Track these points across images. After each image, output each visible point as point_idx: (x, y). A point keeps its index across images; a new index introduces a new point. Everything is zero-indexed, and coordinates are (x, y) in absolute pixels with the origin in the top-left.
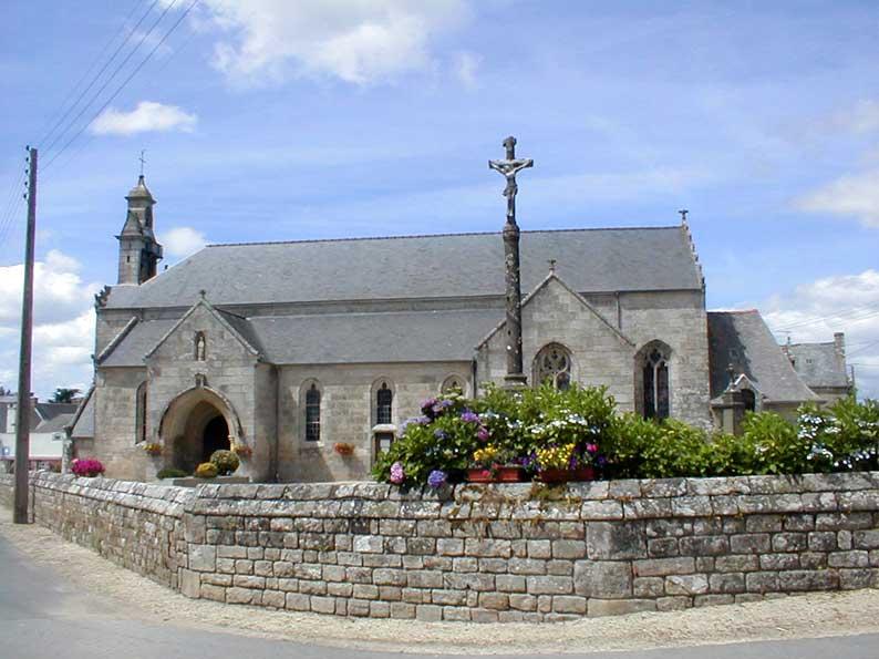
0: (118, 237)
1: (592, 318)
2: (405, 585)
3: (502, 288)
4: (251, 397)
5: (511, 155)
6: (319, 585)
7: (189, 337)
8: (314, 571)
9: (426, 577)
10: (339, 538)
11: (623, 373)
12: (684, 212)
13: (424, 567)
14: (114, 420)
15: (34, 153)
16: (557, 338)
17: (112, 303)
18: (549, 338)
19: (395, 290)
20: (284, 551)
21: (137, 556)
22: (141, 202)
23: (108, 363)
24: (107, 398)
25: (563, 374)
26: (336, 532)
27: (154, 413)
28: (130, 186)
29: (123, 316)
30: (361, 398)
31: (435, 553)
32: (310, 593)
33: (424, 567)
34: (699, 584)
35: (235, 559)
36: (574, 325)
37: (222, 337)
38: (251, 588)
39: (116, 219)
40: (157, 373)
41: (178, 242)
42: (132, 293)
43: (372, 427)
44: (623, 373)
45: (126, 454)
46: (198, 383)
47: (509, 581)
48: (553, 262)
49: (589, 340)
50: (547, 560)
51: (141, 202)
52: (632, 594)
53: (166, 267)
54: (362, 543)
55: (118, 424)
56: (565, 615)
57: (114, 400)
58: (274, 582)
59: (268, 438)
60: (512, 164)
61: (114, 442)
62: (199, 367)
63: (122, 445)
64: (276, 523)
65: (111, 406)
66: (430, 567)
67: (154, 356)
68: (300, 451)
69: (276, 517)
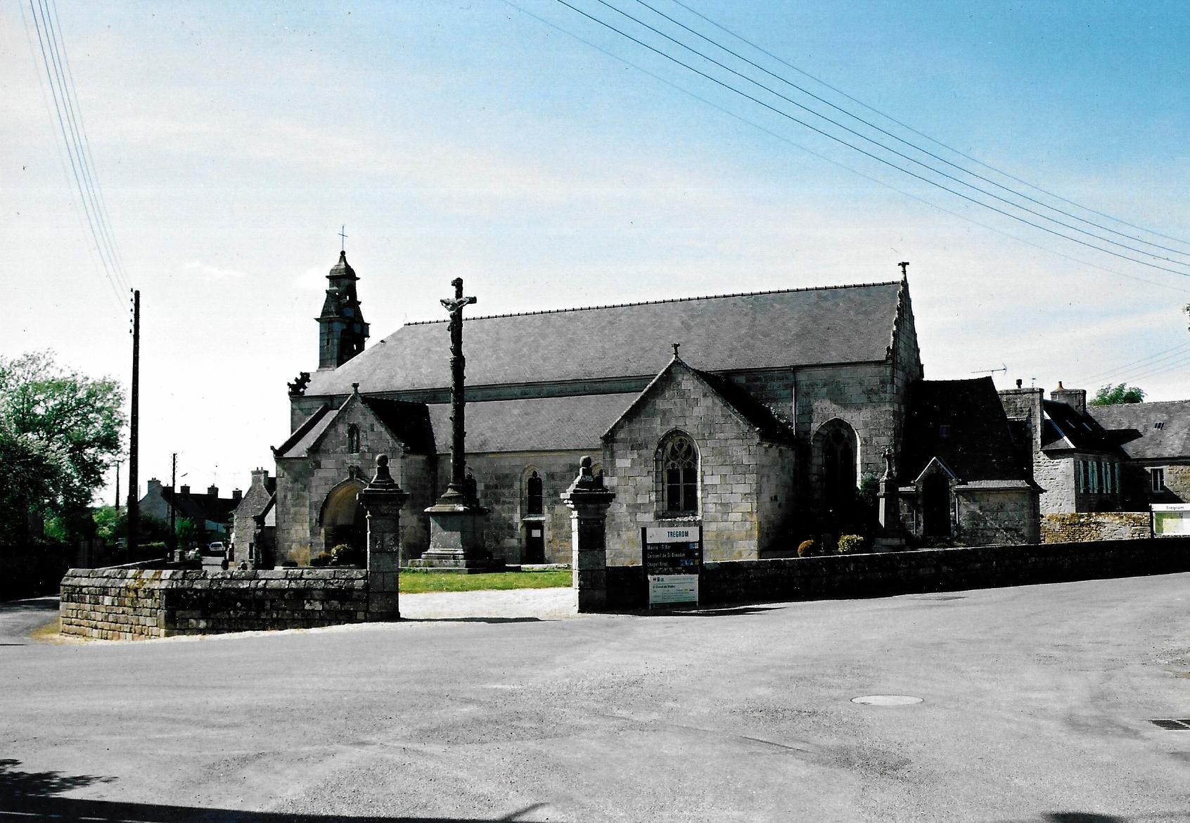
3: (469, 408)
7: (343, 429)
11: (745, 462)
12: (904, 265)
15: (137, 294)
17: (311, 389)
18: (672, 426)
19: (571, 369)
21: (99, 616)
22: (343, 282)
23: (291, 453)
25: (689, 464)
28: (333, 262)
30: (511, 486)
34: (203, 624)
36: (698, 411)
41: (381, 314)
42: (338, 380)
44: (745, 462)
46: (352, 474)
49: (710, 426)
51: (343, 282)
52: (175, 625)
54: (107, 600)
55: (295, 514)
57: (292, 490)
61: (293, 531)
62: (354, 460)
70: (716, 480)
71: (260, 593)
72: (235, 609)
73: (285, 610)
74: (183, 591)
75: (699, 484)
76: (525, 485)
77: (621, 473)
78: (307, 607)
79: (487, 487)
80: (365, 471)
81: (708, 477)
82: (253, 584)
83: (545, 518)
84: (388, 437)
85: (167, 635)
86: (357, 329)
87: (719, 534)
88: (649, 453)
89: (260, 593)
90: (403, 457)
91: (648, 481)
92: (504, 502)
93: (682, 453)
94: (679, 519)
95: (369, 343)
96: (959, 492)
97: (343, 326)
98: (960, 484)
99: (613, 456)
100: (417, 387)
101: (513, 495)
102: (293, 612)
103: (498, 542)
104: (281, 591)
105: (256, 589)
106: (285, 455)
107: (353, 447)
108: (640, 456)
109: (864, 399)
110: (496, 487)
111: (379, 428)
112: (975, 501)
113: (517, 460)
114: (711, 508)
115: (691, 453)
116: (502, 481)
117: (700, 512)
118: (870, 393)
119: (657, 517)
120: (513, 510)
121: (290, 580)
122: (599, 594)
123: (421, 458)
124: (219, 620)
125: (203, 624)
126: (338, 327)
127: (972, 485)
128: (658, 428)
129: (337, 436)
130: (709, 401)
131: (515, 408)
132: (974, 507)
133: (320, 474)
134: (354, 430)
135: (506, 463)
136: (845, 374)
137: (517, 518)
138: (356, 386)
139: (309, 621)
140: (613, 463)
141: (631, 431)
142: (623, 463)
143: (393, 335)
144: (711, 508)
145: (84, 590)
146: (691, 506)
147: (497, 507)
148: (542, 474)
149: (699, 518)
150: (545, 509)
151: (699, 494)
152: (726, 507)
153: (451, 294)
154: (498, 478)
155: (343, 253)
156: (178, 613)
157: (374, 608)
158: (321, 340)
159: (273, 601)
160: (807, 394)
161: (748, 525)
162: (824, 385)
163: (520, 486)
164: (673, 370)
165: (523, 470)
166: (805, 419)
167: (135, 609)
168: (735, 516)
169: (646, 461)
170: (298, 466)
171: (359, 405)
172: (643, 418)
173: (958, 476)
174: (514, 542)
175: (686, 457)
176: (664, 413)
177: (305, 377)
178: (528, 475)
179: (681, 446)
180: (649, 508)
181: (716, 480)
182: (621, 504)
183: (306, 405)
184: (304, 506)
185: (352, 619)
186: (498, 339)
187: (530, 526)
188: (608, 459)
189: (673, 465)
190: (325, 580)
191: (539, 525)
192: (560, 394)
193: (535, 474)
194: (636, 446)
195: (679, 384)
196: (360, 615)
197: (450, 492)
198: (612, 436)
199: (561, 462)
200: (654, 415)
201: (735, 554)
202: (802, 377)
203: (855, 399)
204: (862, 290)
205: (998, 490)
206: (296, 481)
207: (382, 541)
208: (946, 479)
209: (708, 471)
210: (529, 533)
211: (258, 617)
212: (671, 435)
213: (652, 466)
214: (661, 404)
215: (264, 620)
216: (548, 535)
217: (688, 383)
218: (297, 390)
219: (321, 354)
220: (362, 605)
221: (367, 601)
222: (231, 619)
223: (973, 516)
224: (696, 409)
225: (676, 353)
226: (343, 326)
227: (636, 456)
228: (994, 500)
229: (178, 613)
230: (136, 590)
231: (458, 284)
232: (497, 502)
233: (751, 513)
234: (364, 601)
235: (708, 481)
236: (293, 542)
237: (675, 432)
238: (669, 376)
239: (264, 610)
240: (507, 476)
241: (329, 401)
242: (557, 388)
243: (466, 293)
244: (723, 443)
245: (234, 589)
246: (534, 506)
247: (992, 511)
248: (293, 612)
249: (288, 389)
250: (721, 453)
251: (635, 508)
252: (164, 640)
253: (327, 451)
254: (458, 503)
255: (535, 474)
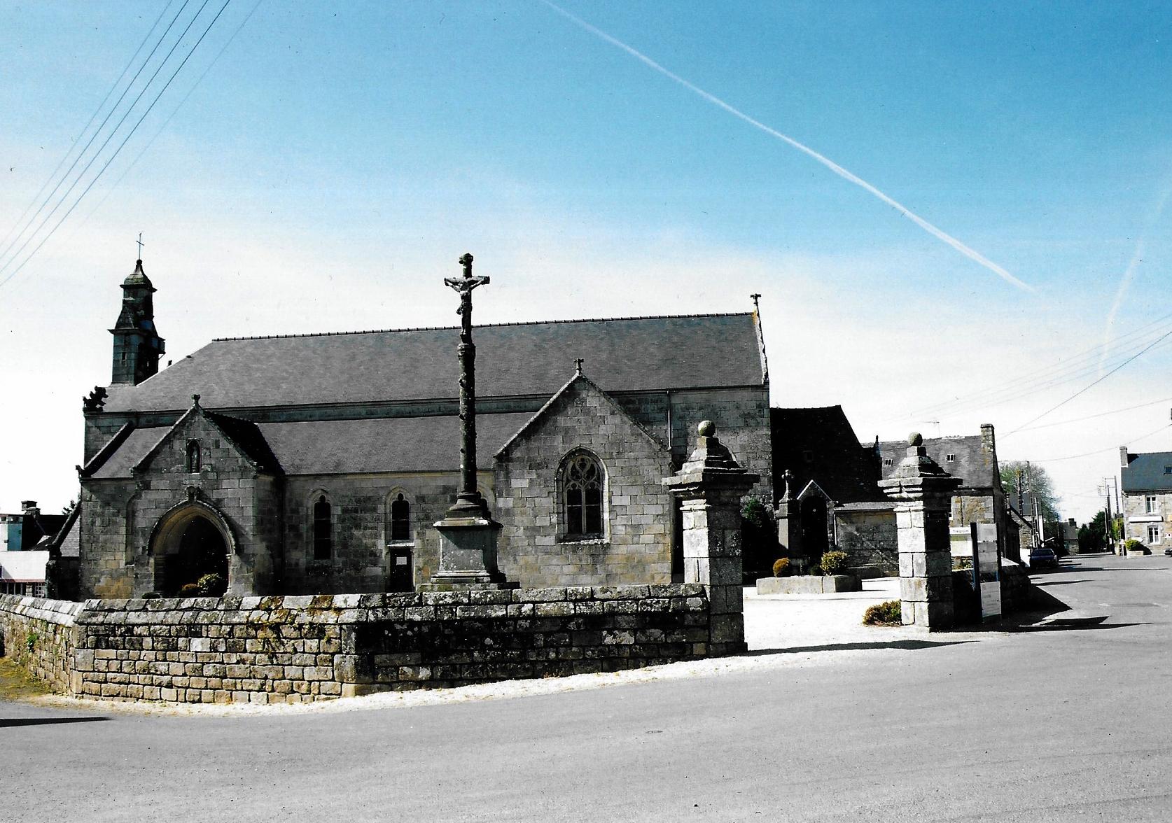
0: (111, 331)
1: (623, 422)
2: (225, 677)
4: (250, 511)
5: (468, 273)
6: (166, 679)
7: (179, 446)
8: (162, 667)
9: (239, 670)
10: (180, 640)
12: (756, 297)
13: (238, 662)
14: (102, 538)
16: (585, 443)
17: (109, 406)
18: (576, 444)
20: (143, 653)
22: (139, 294)
23: (101, 473)
24: (94, 514)
25: (592, 485)
26: (178, 637)
27: (143, 530)
29: (117, 421)
30: (375, 510)
31: (245, 651)
32: (160, 685)
33: (238, 662)
34: (424, 673)
35: (109, 660)
37: (218, 447)
38: (120, 683)
39: (112, 307)
40: (147, 486)
41: (180, 332)
42: (124, 397)
43: (387, 542)
45: (115, 576)
46: (191, 496)
47: (292, 672)
48: (580, 361)
49: (618, 447)
50: (317, 654)
51: (139, 294)
52: (371, 676)
53: (170, 363)
54: (197, 644)
55: (105, 541)
56: (329, 696)
58: (134, 678)
59: (272, 556)
60: (467, 286)
61: (102, 562)
62: (194, 480)
63: (114, 560)
64: (137, 630)
65: (98, 522)
66: (242, 661)
67: (144, 469)
68: (308, 570)
69: (139, 625)
70: (626, 501)
71: (526, 624)
72: (483, 649)
73: (570, 646)
74: (388, 624)
75: (606, 505)
76: (389, 508)
77: (517, 493)
78: (609, 640)
79: (345, 511)
80: (208, 493)
81: (617, 500)
82: (512, 610)
83: (414, 543)
84: (237, 454)
85: (360, 692)
86: (155, 344)
87: (629, 558)
88: (551, 472)
89: (526, 624)
90: (255, 478)
91: (548, 503)
92: (366, 528)
93: (583, 473)
94: (582, 542)
95: (162, 364)
96: (838, 514)
97: (137, 340)
98: (837, 506)
99: (507, 476)
100: (242, 404)
101: (378, 520)
102: (584, 648)
103: (357, 569)
104: (566, 619)
105: (515, 619)
106: (94, 476)
107: (193, 465)
108: (539, 476)
109: (741, 423)
110: (356, 511)
111: (224, 444)
112: (852, 523)
113: (381, 482)
114: (621, 530)
115: (595, 474)
116: (366, 503)
117: (607, 535)
118: (746, 417)
119: (559, 540)
120: (376, 536)
121: (575, 602)
122: (948, 608)
123: (269, 479)
124: (453, 665)
125: (424, 673)
126: (135, 340)
127: (848, 507)
128: (560, 447)
129: (172, 453)
130: (617, 420)
131: (364, 430)
132: (851, 529)
133: (148, 496)
134: (193, 446)
135: (368, 485)
136: (721, 398)
137: (381, 544)
138: (197, 398)
139: (612, 661)
140: (508, 483)
141: (529, 450)
142: (520, 483)
143: (201, 351)
144: (621, 530)
145: (137, 630)
146: (596, 527)
147: (356, 533)
148: (409, 497)
149: (606, 541)
150: (415, 534)
151: (606, 516)
152: (637, 528)
153: (458, 273)
154: (358, 501)
155: (139, 262)
156: (378, 659)
157: (718, 637)
158: (115, 354)
159: (547, 634)
160: (682, 418)
161: (660, 547)
162: (700, 409)
163: (385, 509)
164: (576, 385)
165: (386, 491)
166: (680, 442)
167: (273, 655)
168: (647, 538)
169: (546, 481)
170: (110, 489)
171: (200, 419)
172: (542, 435)
173: (834, 500)
174: (378, 570)
175: (588, 478)
176: (567, 430)
177: (100, 393)
178: (393, 497)
179: (583, 466)
180: (549, 531)
181: (626, 501)
182: (518, 528)
183: (105, 422)
184: (117, 533)
185: (683, 653)
186: (328, 358)
187: (395, 553)
188: (502, 479)
189: (574, 486)
190: (636, 600)
191: (407, 552)
192: (411, 415)
193: (401, 496)
194: (534, 466)
195: (583, 401)
196: (699, 648)
197: (461, 503)
198: (507, 454)
199: (433, 484)
200: (555, 433)
201: (648, 577)
202: (677, 400)
203: (731, 423)
204: (716, 319)
205: (875, 512)
206: (106, 504)
207: (724, 542)
208: (824, 502)
209: (616, 491)
210: (393, 561)
211: (523, 659)
212: (572, 454)
213: (552, 486)
214: (562, 421)
215: (533, 663)
216: (417, 562)
217: (593, 401)
218: (94, 404)
219: (115, 369)
220: (701, 634)
221: (707, 627)
222: (474, 663)
223: (850, 538)
224: (603, 427)
225: (580, 369)
226: (137, 340)
227: (535, 476)
228: (870, 521)
229: (378, 659)
230: (276, 627)
231: (467, 261)
232: (358, 527)
233: (664, 535)
234: (703, 627)
235: (617, 501)
236: (102, 574)
237: (580, 450)
238: (571, 394)
239: (533, 648)
240: (369, 498)
241: (135, 420)
242: (423, 408)
243: (475, 273)
244: (633, 463)
245: (479, 619)
246: (400, 529)
247: (868, 532)
248: (584, 648)
249: (82, 405)
250: (632, 473)
251: (533, 531)
252: (351, 702)
253: (159, 471)
254: (477, 515)
255: (401, 496)
